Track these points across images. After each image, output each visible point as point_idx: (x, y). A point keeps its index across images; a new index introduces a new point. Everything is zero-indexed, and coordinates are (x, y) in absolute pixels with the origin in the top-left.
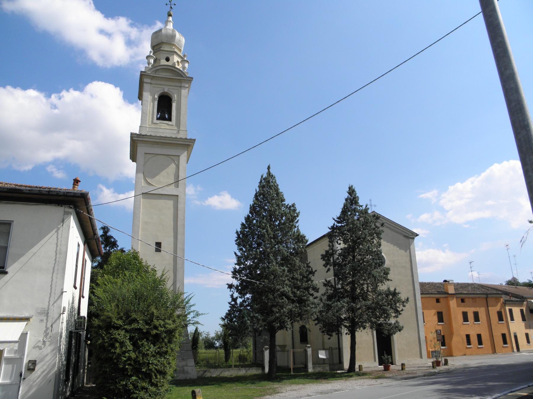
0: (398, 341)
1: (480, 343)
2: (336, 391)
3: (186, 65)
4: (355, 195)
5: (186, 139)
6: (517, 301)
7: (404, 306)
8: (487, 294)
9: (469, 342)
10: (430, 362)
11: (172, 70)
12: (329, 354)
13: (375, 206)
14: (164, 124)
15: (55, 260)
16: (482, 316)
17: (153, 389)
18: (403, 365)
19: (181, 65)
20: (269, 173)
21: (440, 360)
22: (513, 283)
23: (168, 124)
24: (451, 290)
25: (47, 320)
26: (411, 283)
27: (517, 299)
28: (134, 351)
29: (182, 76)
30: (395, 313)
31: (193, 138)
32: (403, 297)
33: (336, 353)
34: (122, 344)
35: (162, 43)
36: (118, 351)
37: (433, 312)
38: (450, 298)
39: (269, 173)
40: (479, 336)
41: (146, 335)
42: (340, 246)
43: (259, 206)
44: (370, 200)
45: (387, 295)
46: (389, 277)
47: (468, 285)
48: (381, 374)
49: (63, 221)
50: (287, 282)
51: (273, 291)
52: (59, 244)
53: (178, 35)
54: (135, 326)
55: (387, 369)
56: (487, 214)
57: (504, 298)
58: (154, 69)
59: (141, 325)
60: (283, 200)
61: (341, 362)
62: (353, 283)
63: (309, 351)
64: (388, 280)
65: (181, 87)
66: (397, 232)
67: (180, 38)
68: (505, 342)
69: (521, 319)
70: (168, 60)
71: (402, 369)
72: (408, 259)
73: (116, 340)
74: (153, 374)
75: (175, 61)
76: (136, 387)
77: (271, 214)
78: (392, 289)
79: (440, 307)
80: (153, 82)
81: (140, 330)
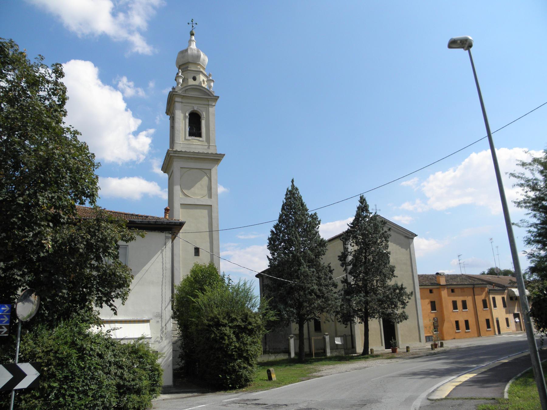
0: (401, 328)
1: (467, 327)
2: (365, 367)
3: (212, 84)
4: (366, 204)
5: (216, 154)
6: (499, 290)
7: (409, 299)
8: (474, 285)
9: (458, 328)
10: (429, 345)
11: (200, 89)
12: (344, 340)
13: (380, 210)
14: (195, 140)
15: (163, 275)
16: (470, 304)
17: (249, 367)
18: (408, 348)
19: (206, 83)
20: (293, 186)
21: (437, 343)
22: (492, 272)
23: (199, 140)
24: (443, 282)
25: (162, 321)
26: (411, 278)
27: (499, 288)
28: (237, 342)
29: (209, 96)
30: (402, 304)
31: (223, 153)
32: (408, 291)
33: (350, 340)
34: (229, 337)
35: (189, 63)
36: (227, 342)
37: (427, 301)
38: (441, 289)
39: (293, 186)
40: (467, 322)
41: (243, 330)
42: (352, 248)
43: (286, 215)
44: (376, 205)
45: (395, 290)
46: (395, 273)
47: (457, 276)
48: (390, 355)
49: (165, 244)
50: (314, 281)
51: (303, 289)
52: (164, 262)
53: (202, 55)
54: (235, 323)
55: (394, 351)
56: (467, 200)
57: (489, 287)
58: (184, 89)
59: (239, 323)
60: (307, 210)
61: (353, 347)
62: (363, 279)
63: (327, 338)
64: (394, 276)
65: (208, 105)
66: (399, 233)
67: (204, 58)
68: (489, 327)
69: (502, 305)
70: (194, 79)
71: (407, 351)
72: (409, 256)
73: (225, 335)
74: (250, 358)
75: (201, 80)
76: (240, 367)
77: (299, 223)
78: (399, 284)
79: (433, 297)
80: (184, 101)
81: (239, 327)
